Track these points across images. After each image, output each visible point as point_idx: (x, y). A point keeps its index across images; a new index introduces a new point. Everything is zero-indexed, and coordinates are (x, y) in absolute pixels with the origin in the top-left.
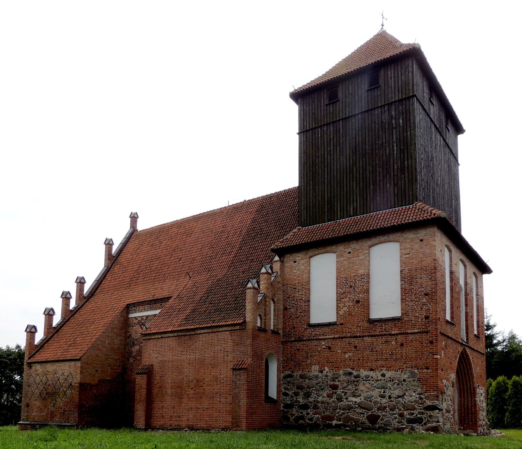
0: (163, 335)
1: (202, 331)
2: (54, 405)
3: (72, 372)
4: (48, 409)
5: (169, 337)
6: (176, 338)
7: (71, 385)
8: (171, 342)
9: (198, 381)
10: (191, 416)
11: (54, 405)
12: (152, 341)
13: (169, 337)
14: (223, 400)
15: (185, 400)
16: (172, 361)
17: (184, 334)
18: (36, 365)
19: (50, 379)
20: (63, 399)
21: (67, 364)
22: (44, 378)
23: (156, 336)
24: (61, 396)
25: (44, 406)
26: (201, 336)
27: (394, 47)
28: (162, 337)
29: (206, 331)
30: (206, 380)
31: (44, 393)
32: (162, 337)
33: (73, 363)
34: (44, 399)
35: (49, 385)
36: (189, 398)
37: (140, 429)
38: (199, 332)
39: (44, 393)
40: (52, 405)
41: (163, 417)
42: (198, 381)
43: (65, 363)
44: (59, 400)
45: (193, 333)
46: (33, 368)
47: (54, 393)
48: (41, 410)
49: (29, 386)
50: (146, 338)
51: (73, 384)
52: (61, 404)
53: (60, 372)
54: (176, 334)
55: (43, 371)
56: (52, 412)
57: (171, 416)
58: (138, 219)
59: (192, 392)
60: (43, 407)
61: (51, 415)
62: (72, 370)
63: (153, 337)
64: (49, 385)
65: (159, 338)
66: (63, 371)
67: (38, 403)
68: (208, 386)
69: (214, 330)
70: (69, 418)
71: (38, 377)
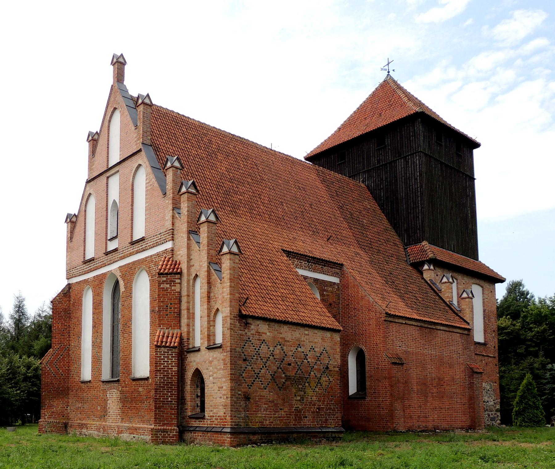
0: (407, 321)
1: (442, 328)
2: (302, 398)
3: (327, 349)
4: (291, 406)
5: (412, 325)
6: (418, 328)
7: (327, 368)
8: (413, 331)
9: (439, 379)
10: (436, 416)
11: (302, 398)
12: (394, 325)
13: (412, 325)
14: (459, 400)
15: (430, 399)
16: (416, 353)
17: (426, 326)
18: (258, 322)
19: (290, 353)
20: (317, 389)
21: (320, 333)
22: (277, 351)
23: (400, 321)
24: (313, 384)
25: (283, 400)
26: (439, 332)
27: (403, 105)
28: (405, 324)
29: (444, 328)
30: (446, 379)
31: (282, 378)
32: (405, 324)
33: (328, 334)
34: (283, 387)
35: (290, 364)
36: (433, 397)
37: (401, 432)
38: (439, 327)
39: (282, 378)
40: (299, 398)
41: (411, 417)
42: (439, 379)
43: (316, 331)
44: (309, 391)
45: (434, 327)
46: (252, 327)
47: (302, 378)
48: (275, 407)
49: (245, 360)
50: (390, 319)
51: (331, 368)
52: (314, 398)
53: (308, 346)
54: (419, 324)
55: (274, 337)
56: (298, 411)
57: (419, 417)
58: (126, 67)
59: (435, 390)
60: (280, 402)
61: (296, 415)
62: (327, 345)
63: (396, 321)
64: (290, 364)
65: (402, 323)
66: (312, 344)
67: (268, 394)
68: (448, 385)
69: (451, 330)
70: (327, 420)
71: (264, 347)
